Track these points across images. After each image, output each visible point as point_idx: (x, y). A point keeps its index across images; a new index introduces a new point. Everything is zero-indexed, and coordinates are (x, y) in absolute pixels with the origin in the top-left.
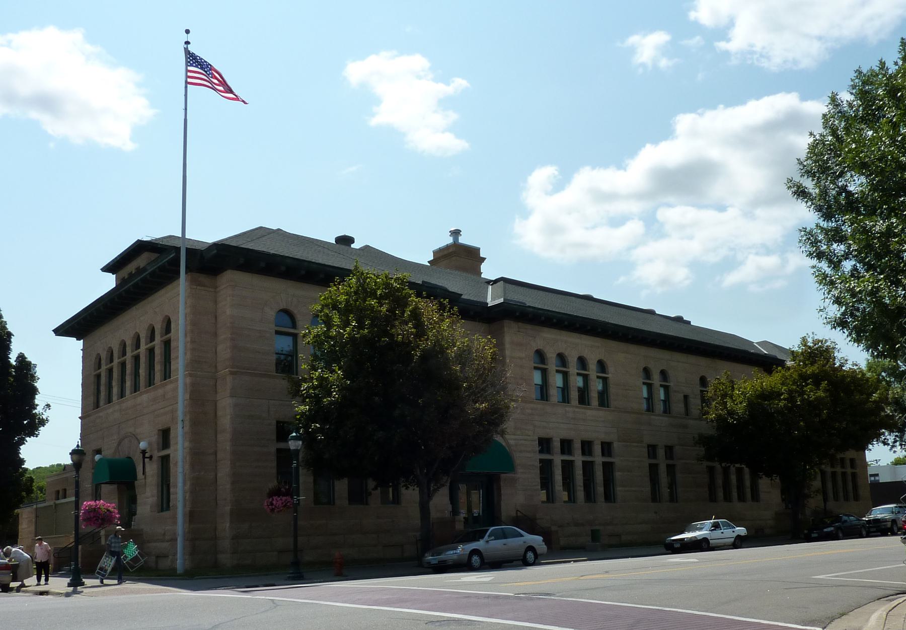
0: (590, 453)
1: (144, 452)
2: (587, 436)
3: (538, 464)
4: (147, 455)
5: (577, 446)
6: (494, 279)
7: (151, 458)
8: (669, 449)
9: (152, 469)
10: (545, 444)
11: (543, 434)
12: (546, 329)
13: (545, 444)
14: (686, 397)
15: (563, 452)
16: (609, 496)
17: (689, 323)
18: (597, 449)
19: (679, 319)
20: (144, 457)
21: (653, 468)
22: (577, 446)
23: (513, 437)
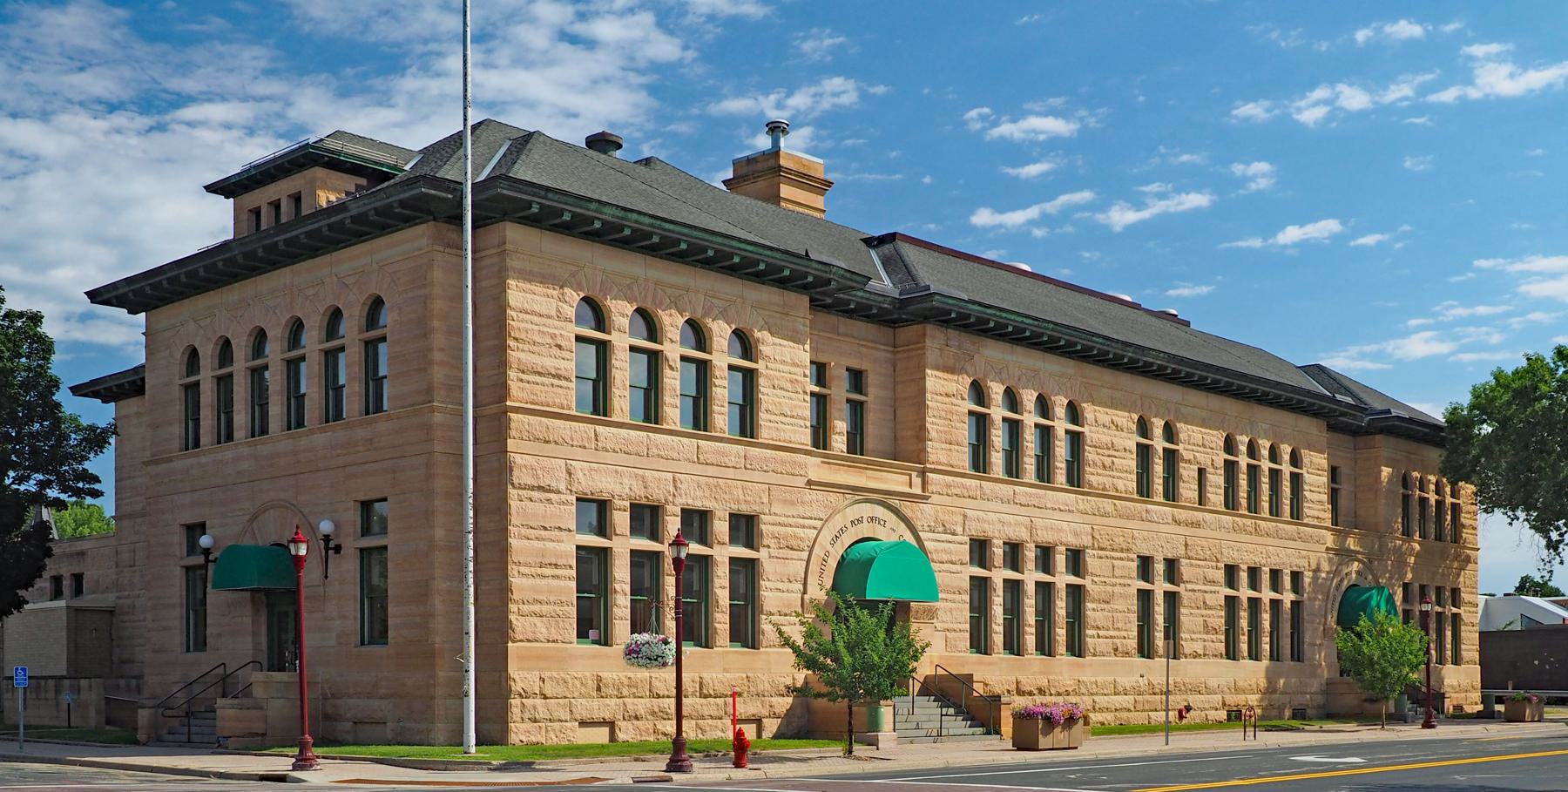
0: (602, 529)
1: (327, 539)
2: (1045, 537)
3: (966, 584)
4: (332, 545)
5: (1030, 554)
6: (877, 234)
7: (338, 549)
8: (1296, 576)
9: (347, 568)
10: (980, 550)
11: (976, 530)
12: (990, 342)
13: (598, 512)
14: (1201, 471)
15: (635, 530)
16: (1076, 647)
17: (1187, 324)
18: (1060, 560)
19: (1317, 371)
20: (327, 549)
21: (1145, 597)
22: (1030, 554)
23: (931, 535)
